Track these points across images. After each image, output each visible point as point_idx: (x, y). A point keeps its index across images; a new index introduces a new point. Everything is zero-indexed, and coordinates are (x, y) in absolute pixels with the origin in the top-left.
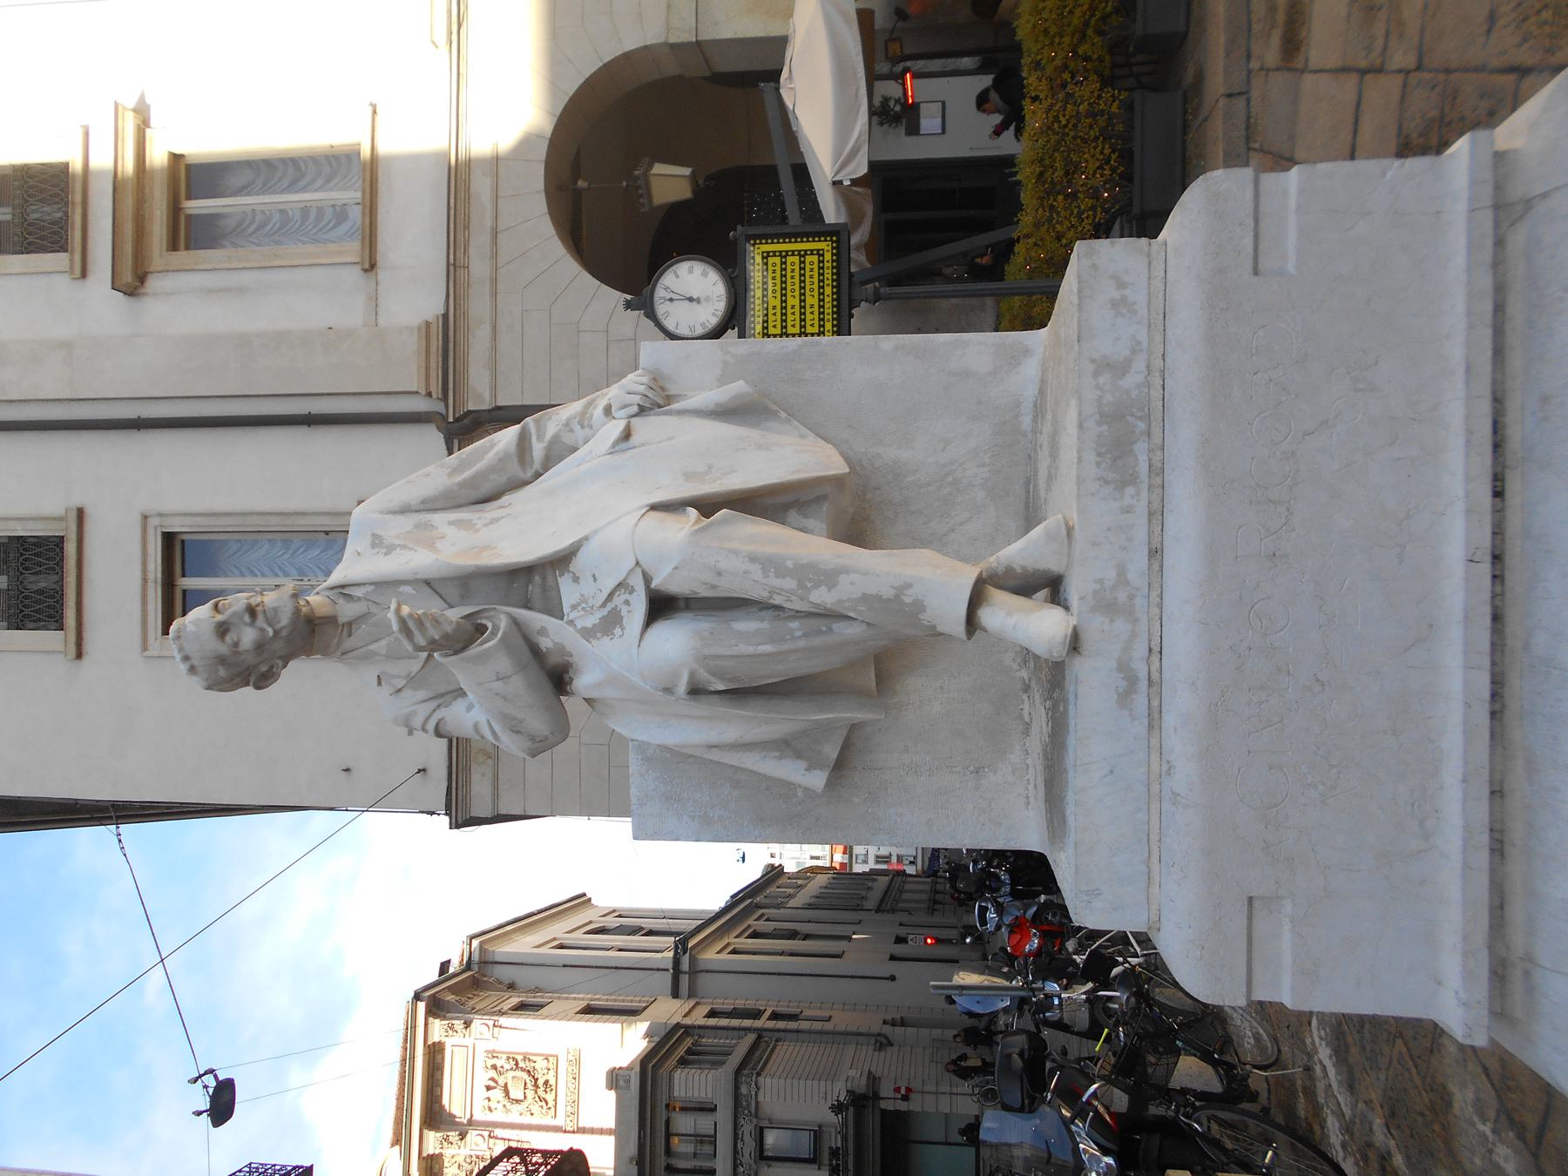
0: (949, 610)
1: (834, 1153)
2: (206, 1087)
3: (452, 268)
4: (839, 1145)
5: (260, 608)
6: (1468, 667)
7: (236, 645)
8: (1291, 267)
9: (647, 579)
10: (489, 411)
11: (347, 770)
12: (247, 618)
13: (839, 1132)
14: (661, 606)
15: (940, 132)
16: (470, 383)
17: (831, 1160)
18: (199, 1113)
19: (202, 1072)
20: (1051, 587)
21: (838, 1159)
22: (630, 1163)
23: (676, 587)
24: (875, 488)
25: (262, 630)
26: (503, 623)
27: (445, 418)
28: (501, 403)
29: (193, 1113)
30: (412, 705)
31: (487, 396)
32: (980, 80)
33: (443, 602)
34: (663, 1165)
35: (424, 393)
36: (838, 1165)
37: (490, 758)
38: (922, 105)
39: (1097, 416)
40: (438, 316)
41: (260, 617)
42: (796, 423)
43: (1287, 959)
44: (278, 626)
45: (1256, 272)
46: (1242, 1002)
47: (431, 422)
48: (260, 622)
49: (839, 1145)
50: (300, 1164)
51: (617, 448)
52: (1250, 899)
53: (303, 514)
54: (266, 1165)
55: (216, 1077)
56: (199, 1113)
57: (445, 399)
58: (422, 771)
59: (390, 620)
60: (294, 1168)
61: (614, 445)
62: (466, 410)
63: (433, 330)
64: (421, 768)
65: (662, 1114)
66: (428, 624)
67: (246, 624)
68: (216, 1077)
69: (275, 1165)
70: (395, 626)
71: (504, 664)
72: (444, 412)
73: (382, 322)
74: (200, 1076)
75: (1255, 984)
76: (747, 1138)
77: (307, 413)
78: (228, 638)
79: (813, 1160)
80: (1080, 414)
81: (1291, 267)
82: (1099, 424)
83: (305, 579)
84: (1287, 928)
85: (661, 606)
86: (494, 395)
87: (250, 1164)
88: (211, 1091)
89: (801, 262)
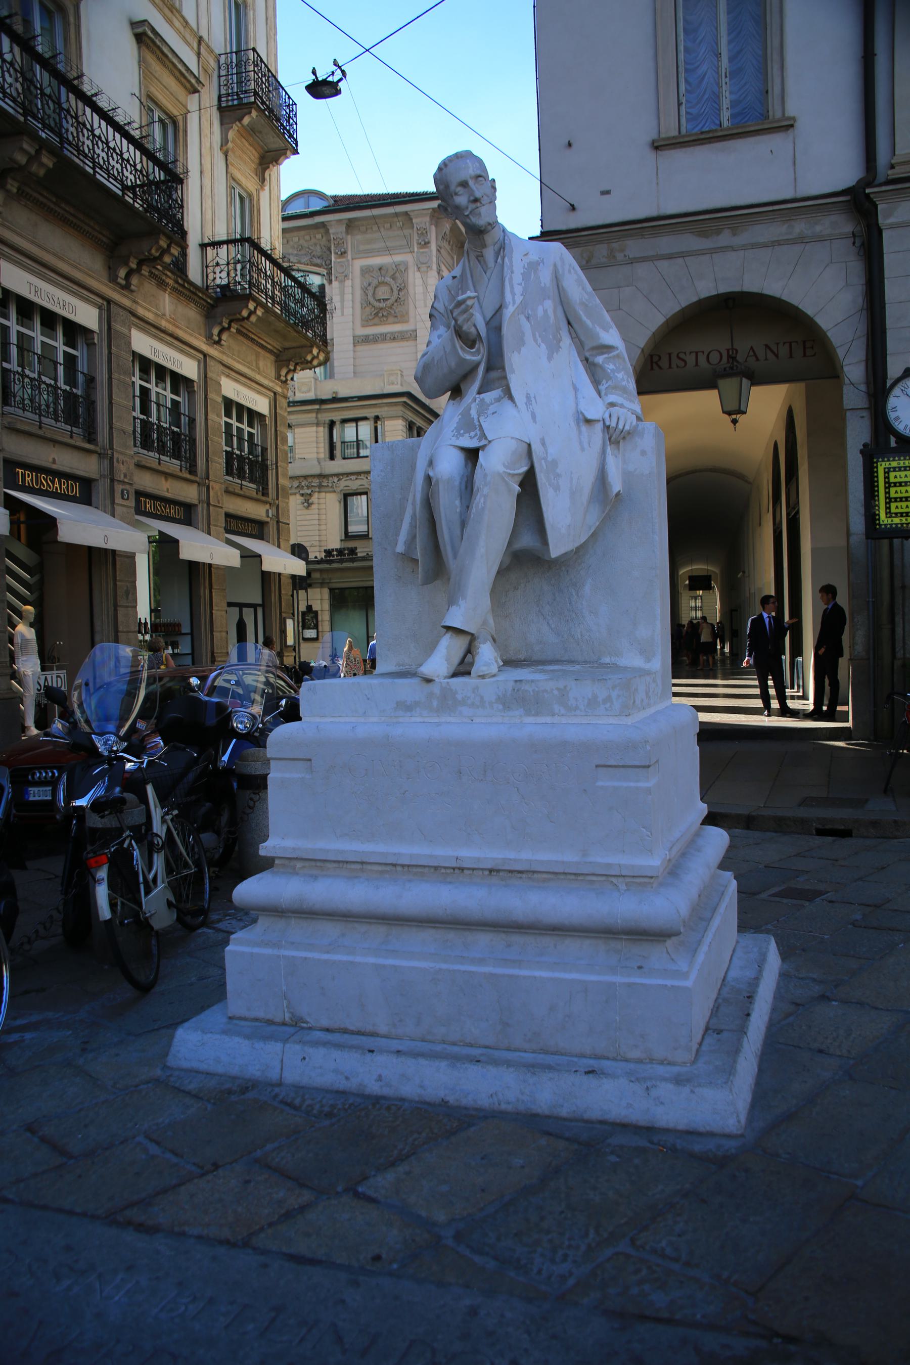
0: (456, 618)
1: (353, 551)
2: (333, 73)
4: (359, 555)
5: (478, 204)
7: (456, 194)
8: (600, 783)
9: (483, 447)
10: (877, 224)
11: (570, 145)
12: (472, 198)
13: (368, 554)
14: (472, 455)
17: (348, 549)
18: (314, 72)
19: (343, 68)
20: (463, 669)
21: (349, 555)
22: (334, 393)
24: (568, 571)
25: (467, 208)
26: (476, 358)
27: (870, 184)
28: (885, 234)
29: (314, 68)
33: (491, 315)
34: (334, 419)
35: (893, 162)
36: (344, 555)
37: (587, 262)
39: (537, 689)
42: (598, 523)
43: (287, 775)
44: (471, 217)
45: (597, 766)
46: (268, 756)
47: (867, 171)
48: (472, 206)
49: (359, 555)
50: (299, 143)
51: (581, 416)
52: (310, 760)
53: (782, 68)
54: (296, 117)
55: (341, 80)
56: (314, 72)
58: (573, 208)
59: (466, 293)
60: (296, 140)
61: (582, 413)
64: (576, 206)
65: (371, 413)
66: (465, 316)
67: (469, 197)
68: (341, 80)
69: (296, 124)
70: (460, 298)
72: (877, 182)
74: (340, 67)
75: (277, 761)
76: (359, 482)
79: (347, 536)
80: (538, 681)
81: (600, 783)
82: (533, 691)
83: (727, 80)
86: (892, 227)
87: (296, 104)
88: (330, 79)
89: (896, 501)
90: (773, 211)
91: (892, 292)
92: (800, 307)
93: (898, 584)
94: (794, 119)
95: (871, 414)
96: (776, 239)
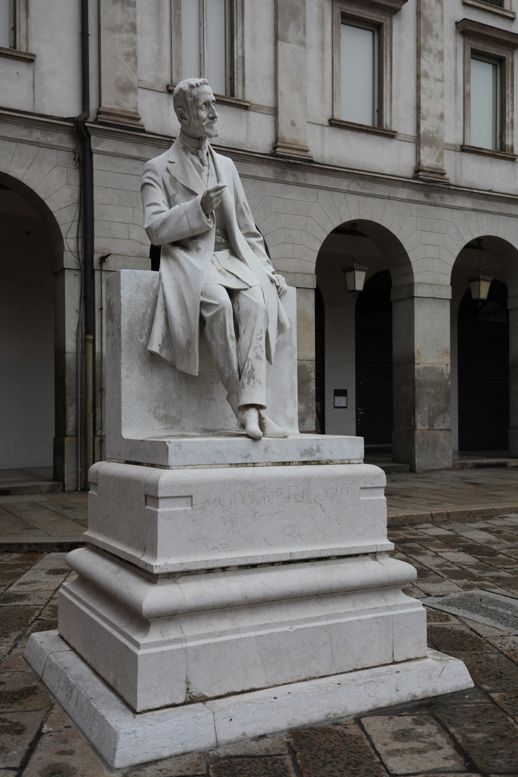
3: (169, 139)
6: (263, 556)
8: (362, 498)
12: (211, 115)
15: (335, 406)
16: (106, 139)
23: (241, 299)
25: (205, 121)
28: (95, 156)
30: (161, 175)
31: (98, 148)
32: (353, 419)
38: (346, 397)
40: (143, 126)
41: (210, 121)
43: (173, 509)
44: (205, 127)
57: (96, 122)
62: (91, 134)
63: (135, 122)
71: (195, 224)
73: (140, 92)
77: (89, 34)
78: (204, 106)
81: (148, 507)
84: (184, 508)
85: (232, 293)
86: (100, 153)
90: (20, 117)
91: (98, 196)
92: (35, 190)
93: (98, 387)
94: (34, 56)
95: (82, 274)
96: (19, 138)
